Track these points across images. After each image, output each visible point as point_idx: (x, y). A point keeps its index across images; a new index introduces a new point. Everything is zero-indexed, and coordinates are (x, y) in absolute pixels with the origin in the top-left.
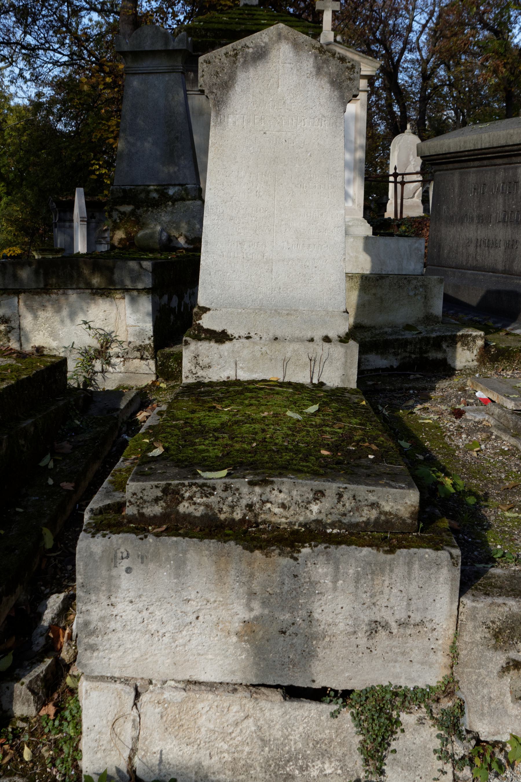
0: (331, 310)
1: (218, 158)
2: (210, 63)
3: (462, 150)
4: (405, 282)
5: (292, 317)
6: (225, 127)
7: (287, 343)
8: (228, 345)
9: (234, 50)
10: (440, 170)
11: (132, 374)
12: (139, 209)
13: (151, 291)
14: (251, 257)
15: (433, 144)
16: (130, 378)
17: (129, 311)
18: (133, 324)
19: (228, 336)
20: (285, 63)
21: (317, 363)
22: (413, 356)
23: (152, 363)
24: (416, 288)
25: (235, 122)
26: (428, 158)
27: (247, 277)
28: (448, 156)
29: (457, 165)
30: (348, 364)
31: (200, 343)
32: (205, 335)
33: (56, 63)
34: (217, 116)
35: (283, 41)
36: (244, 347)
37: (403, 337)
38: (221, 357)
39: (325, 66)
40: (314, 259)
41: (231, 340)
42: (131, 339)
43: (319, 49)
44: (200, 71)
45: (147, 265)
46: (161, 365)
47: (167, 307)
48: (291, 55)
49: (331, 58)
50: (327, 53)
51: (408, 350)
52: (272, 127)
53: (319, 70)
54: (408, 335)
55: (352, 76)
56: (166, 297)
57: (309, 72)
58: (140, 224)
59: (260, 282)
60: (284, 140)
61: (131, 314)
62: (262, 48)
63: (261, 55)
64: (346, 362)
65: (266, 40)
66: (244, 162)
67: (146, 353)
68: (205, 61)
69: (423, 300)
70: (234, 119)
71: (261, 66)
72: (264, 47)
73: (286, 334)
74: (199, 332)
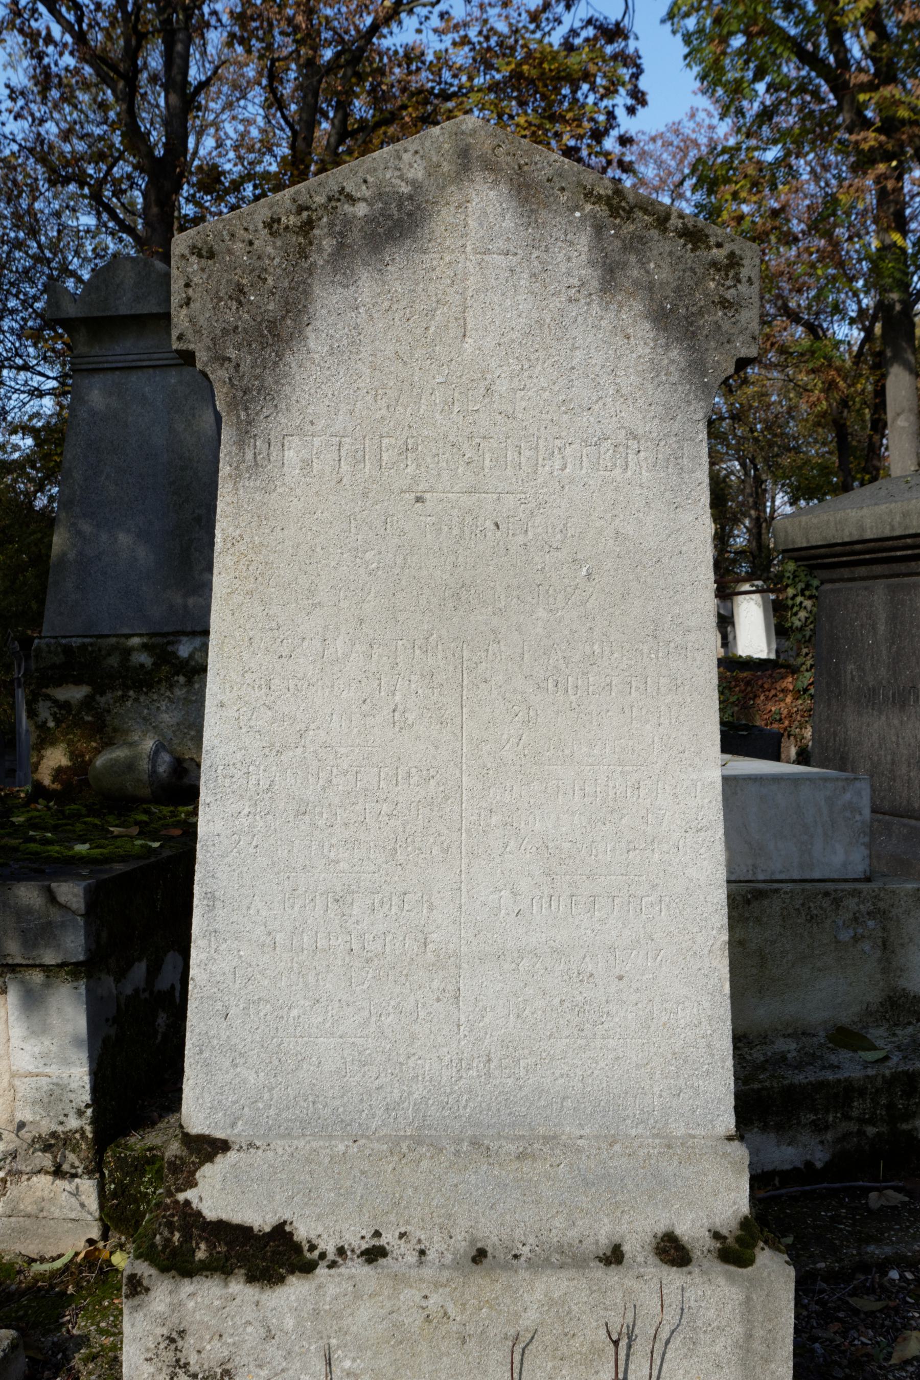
0: (682, 1131)
1: (250, 593)
2: (211, 255)
3: (897, 533)
4: (826, 903)
5: (538, 1165)
6: (271, 479)
7: (523, 1274)
8: (295, 1289)
9: (301, 209)
10: (832, 581)
11: (28, 1221)
12: (102, 694)
13: (82, 970)
14: (377, 947)
15: (815, 521)
16: (23, 1231)
17: (17, 1031)
18: (31, 1068)
19: (297, 1248)
20: (487, 252)
21: (641, 1347)
22: (871, 1131)
23: (88, 1187)
24: (856, 919)
25: (307, 464)
26: (803, 553)
27: (366, 1023)
28: (858, 547)
29: (878, 569)
30: (756, 1345)
31: (187, 1287)
32: (211, 1247)
33: (38, 393)
34: (241, 444)
35: (478, 176)
36: (358, 1297)
37: (840, 1075)
38: (270, 1336)
39: (633, 259)
40: (612, 949)
41: (308, 1268)
42: (25, 1114)
43: (608, 201)
44: (177, 286)
45: (71, 893)
46: (114, 1195)
47: (147, 995)
48: (509, 223)
49: (654, 233)
50: (639, 214)
51: (855, 1113)
52: (445, 476)
53: (610, 274)
54: (851, 1067)
55: (730, 294)
56: (140, 970)
57: (575, 281)
58: (104, 731)
59: (413, 1038)
60: (489, 524)
61: (24, 1039)
62: (401, 199)
63: (399, 224)
64: (749, 1336)
65: (417, 172)
66: (344, 604)
67: (72, 1157)
68: (196, 251)
69: (878, 954)
70: (304, 453)
71: (397, 260)
72: (411, 198)
73: (518, 1234)
74: (187, 1238)
